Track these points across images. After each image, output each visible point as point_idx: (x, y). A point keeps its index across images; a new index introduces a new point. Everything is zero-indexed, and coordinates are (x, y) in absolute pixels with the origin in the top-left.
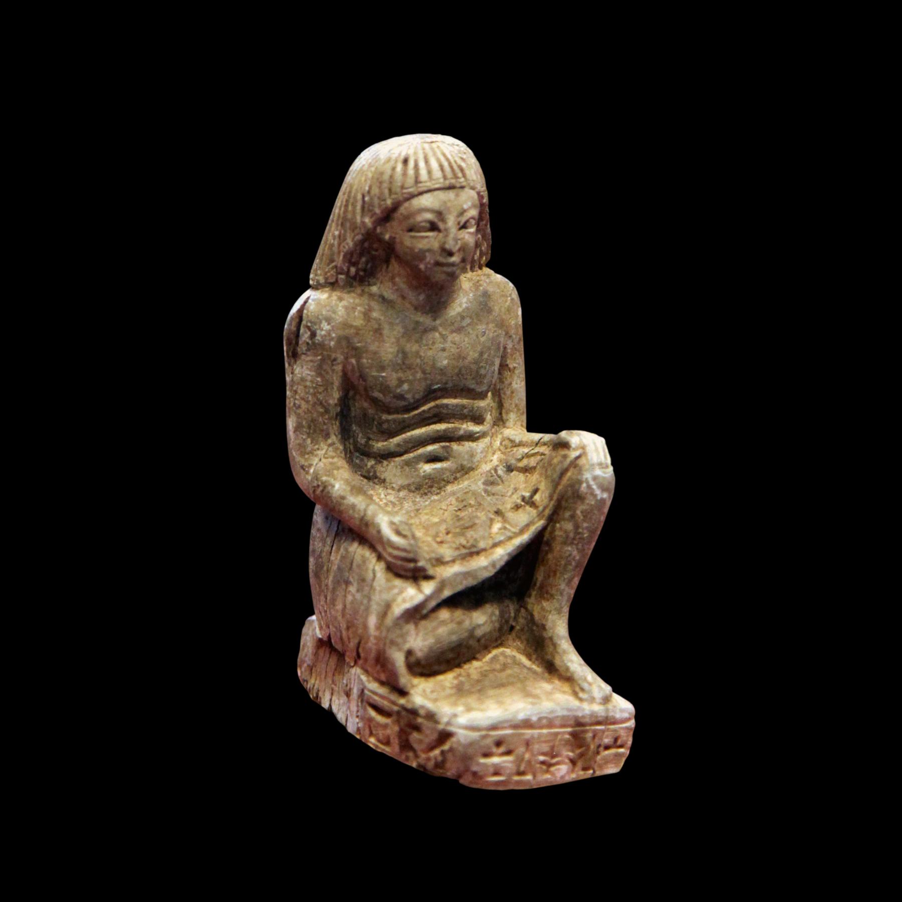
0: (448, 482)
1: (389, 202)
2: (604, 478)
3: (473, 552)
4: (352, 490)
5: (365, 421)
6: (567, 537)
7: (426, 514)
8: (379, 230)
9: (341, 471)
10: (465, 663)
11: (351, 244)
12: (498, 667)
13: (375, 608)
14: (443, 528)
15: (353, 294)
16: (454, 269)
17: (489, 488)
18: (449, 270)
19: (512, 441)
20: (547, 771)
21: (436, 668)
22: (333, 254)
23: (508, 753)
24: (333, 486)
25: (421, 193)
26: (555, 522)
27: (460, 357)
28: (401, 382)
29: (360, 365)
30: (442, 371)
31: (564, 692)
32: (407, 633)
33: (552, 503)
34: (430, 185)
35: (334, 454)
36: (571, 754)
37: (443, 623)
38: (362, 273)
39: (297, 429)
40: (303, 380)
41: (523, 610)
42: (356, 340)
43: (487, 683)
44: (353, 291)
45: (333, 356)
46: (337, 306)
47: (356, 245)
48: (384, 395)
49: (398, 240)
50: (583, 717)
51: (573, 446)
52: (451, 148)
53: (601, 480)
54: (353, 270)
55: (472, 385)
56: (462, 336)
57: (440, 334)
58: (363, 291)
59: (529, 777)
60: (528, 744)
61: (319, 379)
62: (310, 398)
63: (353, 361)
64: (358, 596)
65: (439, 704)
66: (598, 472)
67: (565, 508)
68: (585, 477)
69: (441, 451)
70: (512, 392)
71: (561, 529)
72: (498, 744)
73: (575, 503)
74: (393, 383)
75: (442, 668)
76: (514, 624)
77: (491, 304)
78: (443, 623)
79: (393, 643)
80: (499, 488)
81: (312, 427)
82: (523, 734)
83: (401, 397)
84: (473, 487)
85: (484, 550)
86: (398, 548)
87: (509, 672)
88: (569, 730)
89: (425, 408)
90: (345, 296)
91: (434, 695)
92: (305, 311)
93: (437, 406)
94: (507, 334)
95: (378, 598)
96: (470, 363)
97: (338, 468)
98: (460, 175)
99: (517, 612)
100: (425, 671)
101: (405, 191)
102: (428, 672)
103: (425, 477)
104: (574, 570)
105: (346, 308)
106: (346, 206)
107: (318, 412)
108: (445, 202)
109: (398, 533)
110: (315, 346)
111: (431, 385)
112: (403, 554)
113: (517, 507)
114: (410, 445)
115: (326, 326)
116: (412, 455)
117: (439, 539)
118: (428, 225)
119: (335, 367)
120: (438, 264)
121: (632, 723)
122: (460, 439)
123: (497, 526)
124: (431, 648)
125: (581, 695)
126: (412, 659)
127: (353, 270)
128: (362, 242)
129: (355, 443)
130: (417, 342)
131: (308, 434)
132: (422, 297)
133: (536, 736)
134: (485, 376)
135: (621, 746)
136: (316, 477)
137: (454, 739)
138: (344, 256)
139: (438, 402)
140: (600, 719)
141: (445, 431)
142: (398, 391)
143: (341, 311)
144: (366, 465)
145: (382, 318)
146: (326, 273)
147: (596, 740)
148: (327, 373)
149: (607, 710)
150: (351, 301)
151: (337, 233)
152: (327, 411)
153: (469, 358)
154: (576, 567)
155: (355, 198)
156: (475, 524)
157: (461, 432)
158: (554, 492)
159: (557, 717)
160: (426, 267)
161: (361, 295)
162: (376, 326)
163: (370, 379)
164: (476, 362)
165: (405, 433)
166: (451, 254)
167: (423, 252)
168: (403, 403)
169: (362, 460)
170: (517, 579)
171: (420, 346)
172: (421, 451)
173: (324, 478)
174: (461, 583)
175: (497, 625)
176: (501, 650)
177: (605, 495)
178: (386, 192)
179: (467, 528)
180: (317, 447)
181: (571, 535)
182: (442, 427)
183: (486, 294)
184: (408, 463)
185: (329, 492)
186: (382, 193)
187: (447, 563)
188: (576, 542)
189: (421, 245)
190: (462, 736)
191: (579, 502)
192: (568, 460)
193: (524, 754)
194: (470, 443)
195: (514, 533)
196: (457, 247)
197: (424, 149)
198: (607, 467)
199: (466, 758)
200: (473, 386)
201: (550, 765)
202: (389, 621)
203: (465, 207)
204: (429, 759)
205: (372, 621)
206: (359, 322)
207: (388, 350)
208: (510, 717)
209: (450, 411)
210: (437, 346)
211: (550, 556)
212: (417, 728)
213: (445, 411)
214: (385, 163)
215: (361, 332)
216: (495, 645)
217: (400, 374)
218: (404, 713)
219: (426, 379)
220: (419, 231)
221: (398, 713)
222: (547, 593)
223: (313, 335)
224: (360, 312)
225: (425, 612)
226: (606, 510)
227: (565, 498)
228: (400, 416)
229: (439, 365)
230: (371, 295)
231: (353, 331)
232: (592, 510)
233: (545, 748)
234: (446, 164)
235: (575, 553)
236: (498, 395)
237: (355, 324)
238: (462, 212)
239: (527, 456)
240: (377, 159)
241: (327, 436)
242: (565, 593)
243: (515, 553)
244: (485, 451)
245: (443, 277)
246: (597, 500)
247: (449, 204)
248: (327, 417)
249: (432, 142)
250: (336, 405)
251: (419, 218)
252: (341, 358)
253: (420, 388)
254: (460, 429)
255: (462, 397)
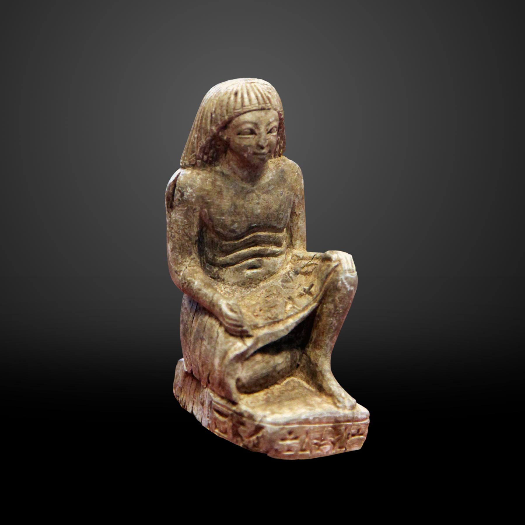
0: (261, 281)
1: (226, 118)
2: (352, 278)
3: (275, 321)
4: (205, 285)
5: (213, 245)
6: (330, 312)
7: (248, 299)
8: (220, 134)
9: (198, 274)
10: (271, 386)
11: (204, 142)
12: (290, 388)
13: (218, 354)
14: (258, 307)
15: (205, 171)
16: (265, 156)
17: (285, 284)
18: (262, 157)
19: (298, 257)
20: (319, 449)
21: (254, 389)
22: (194, 148)
23: (296, 438)
24: (194, 283)
25: (245, 113)
26: (323, 304)
27: (268, 208)
28: (233, 222)
29: (209, 213)
30: (257, 216)
31: (328, 403)
32: (237, 368)
33: (322, 292)
34: (250, 108)
35: (194, 264)
36: (332, 439)
37: (258, 362)
38: (210, 159)
39: (173, 250)
40: (176, 221)
41: (304, 355)
42: (207, 198)
43: (283, 397)
44: (206, 170)
45: (194, 207)
46: (196, 178)
47: (207, 143)
48: (224, 230)
49: (231, 140)
50: (339, 417)
51: (334, 259)
52: (262, 86)
53: (350, 280)
54: (205, 157)
55: (275, 224)
56: (269, 195)
57: (256, 194)
58: (211, 169)
59: (308, 452)
60: (307, 433)
61: (186, 221)
62: (180, 232)
63: (206, 210)
64: (209, 347)
65: (255, 410)
66: (348, 275)
67: (329, 296)
68: (340, 278)
69: (257, 262)
70: (298, 228)
71: (326, 308)
72: (290, 433)
73: (335, 293)
74: (229, 223)
75: (257, 389)
76: (299, 363)
77: (286, 177)
78: (258, 362)
79: (228, 374)
80: (290, 284)
81: (182, 249)
82: (305, 427)
83: (233, 231)
84: (276, 284)
85: (282, 320)
86: (232, 319)
87: (296, 391)
88: (331, 425)
89: (248, 237)
90: (201, 172)
91: (253, 405)
92: (178, 181)
93: (254, 236)
94: (295, 194)
95: (220, 348)
96: (274, 211)
97: (197, 273)
98: (268, 102)
99: (301, 356)
100: (247, 391)
101: (236, 111)
102: (249, 391)
103: (247, 278)
104: (334, 332)
105: (201, 179)
106: (202, 120)
107: (185, 240)
108: (259, 118)
109: (232, 310)
111: (251, 224)
112: (235, 323)
113: (301, 295)
114: (239, 259)
115: (189, 190)
116: (240, 265)
117: (255, 314)
118: (249, 131)
119: (195, 214)
120: (255, 153)
121: (368, 421)
122: (268, 255)
123: (289, 306)
124: (251, 377)
125: (338, 404)
126: (240, 384)
127: (205, 157)
128: (211, 141)
129: (207, 258)
130: (243, 199)
131: (179, 252)
132: (246, 173)
133: (312, 428)
134: (282, 219)
135: (361, 434)
136: (184, 278)
137: (264, 430)
138: (200, 149)
139: (255, 234)
140: (349, 418)
141: (259, 251)
142: (232, 227)
143: (198, 181)
144: (213, 271)
145: (222, 185)
146: (190, 159)
147: (347, 431)
148: (191, 217)
149: (353, 413)
150: (205, 175)
151: (196, 136)
152: (190, 239)
153: (273, 209)
154: (336, 330)
155: (207, 115)
156: (276, 305)
157: (269, 252)
158: (323, 286)
159: (324, 417)
160: (248, 156)
161: (210, 172)
162: (219, 190)
163: (215, 221)
164: (277, 211)
165: (235, 252)
166: (262, 148)
167: (246, 147)
168: (235, 235)
169: (211, 268)
170: (300, 338)
171: (244, 202)
172: (245, 262)
173: (189, 278)
174: (268, 340)
175: (289, 364)
176: (292, 378)
177: (352, 288)
178: (225, 111)
179: (272, 307)
180: (184, 260)
181: (333, 311)
182: (257, 248)
183: (283, 171)
184: (237, 270)
185: (191, 287)
186: (222, 112)
187: (260, 327)
188: (335, 315)
189: (245, 143)
190: (269, 428)
191: (337, 292)
192: (331, 268)
193: (305, 439)
194: (274, 258)
195: (299, 310)
196: (266, 144)
197: (247, 87)
198: (353, 272)
199: (271, 441)
200: (275, 225)
201: (320, 445)
202: (226, 361)
203: (271, 120)
204: (249, 442)
205: (217, 361)
206: (209, 188)
207: (226, 204)
208: (297, 417)
209: (262, 239)
210: (254, 201)
211: (320, 324)
212: (243, 424)
213: (259, 239)
214: (224, 95)
215: (210, 193)
216: (288, 375)
217: (233, 218)
218: (235, 415)
219: (248, 221)
220: (244, 135)
221: (232, 415)
222: (318, 345)
223: (182, 195)
224: (210, 181)
225: (247, 356)
226: (353, 297)
227: (329, 290)
228: (233, 242)
229: (255, 212)
230: (216, 172)
231: (205, 193)
232: (344, 297)
233: (317, 435)
234: (259, 96)
235: (335, 322)
236: (290, 230)
237: (206, 188)
238: (269, 124)
239: (307, 265)
240: (219, 93)
241: (190, 254)
242: (329, 345)
243: (300, 322)
244: (282, 263)
245: (258, 161)
246: (347, 291)
247: (261, 119)
248: (190, 242)
249: (251, 83)
250: (195, 236)
251: (244, 127)
252: (198, 208)
253: (245, 226)
254: (268, 250)
255: (269, 231)
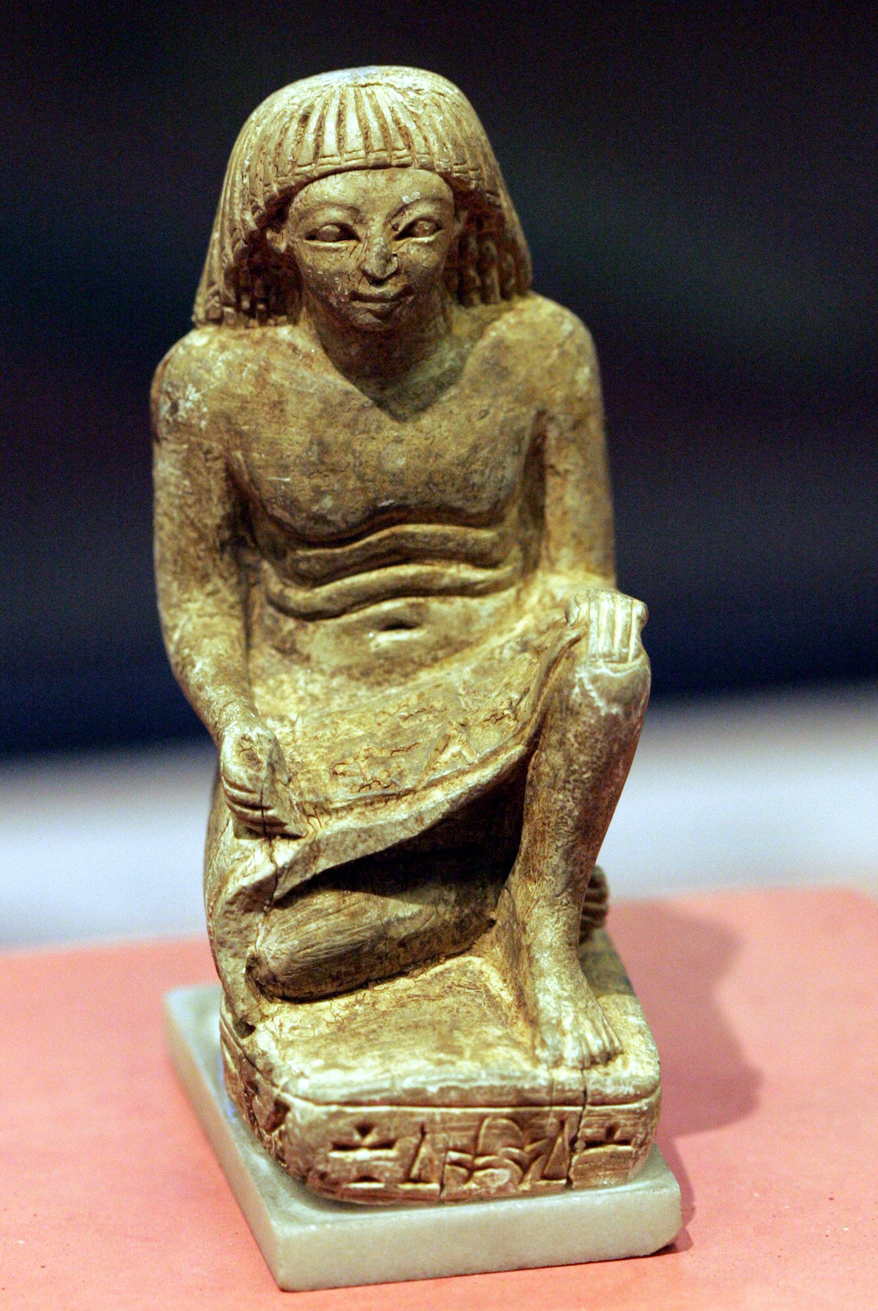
0: (422, 665)
1: (275, 188)
2: (611, 680)
7: (351, 721)
8: (269, 235)
9: (216, 641)
14: (361, 749)
18: (377, 307)
20: (467, 1180)
24: (194, 666)
28: (319, 493)
29: (249, 464)
30: (397, 478)
31: (517, 1045)
33: (536, 715)
34: (338, 161)
37: (321, 914)
42: (241, 419)
45: (206, 443)
46: (215, 359)
47: (239, 256)
48: (292, 515)
50: (533, 1090)
53: (606, 683)
62: (175, 515)
63: (239, 454)
65: (290, 1051)
66: (604, 669)
68: (577, 676)
69: (408, 611)
73: (564, 720)
74: (304, 496)
77: (508, 361)
78: (321, 914)
81: (180, 563)
82: (412, 1115)
83: (320, 519)
87: (449, 1000)
93: (393, 536)
97: (213, 635)
98: (400, 144)
100: (288, 993)
101: (298, 170)
102: (294, 995)
103: (378, 655)
105: (228, 364)
107: (188, 538)
109: (252, 759)
110: (181, 428)
111: (377, 499)
114: (350, 600)
115: (193, 395)
117: (340, 769)
118: (337, 230)
120: (356, 296)
122: (446, 592)
123: (454, 749)
126: (262, 972)
131: (175, 573)
132: (354, 350)
134: (482, 486)
139: (397, 529)
141: (413, 578)
142: (315, 508)
143: (220, 370)
144: (281, 630)
145: (287, 383)
149: (584, 1081)
152: (202, 537)
157: (446, 581)
158: (539, 698)
159: (480, 1088)
162: (276, 397)
163: (266, 486)
164: (462, 463)
165: (341, 578)
171: (353, 434)
172: (372, 610)
174: (355, 847)
176: (462, 960)
180: (186, 596)
181: (562, 774)
182: (409, 570)
184: (348, 630)
185: (186, 676)
187: (337, 810)
190: (302, 1112)
191: (570, 720)
194: (467, 600)
196: (391, 269)
200: (459, 504)
201: (472, 1169)
203: (406, 199)
206: (247, 390)
208: (386, 1085)
209: (420, 545)
210: (385, 433)
213: (411, 545)
215: (249, 406)
217: (315, 481)
218: (244, 1060)
219: (364, 490)
223: (175, 408)
224: (251, 372)
225: (277, 894)
228: (327, 551)
229: (389, 466)
231: (235, 404)
233: (461, 1139)
234: (374, 125)
235: (570, 804)
236: (535, 512)
237: (239, 391)
238: (403, 209)
241: (205, 578)
248: (203, 546)
250: (219, 527)
253: (356, 504)
254: (442, 575)
255: (441, 522)
